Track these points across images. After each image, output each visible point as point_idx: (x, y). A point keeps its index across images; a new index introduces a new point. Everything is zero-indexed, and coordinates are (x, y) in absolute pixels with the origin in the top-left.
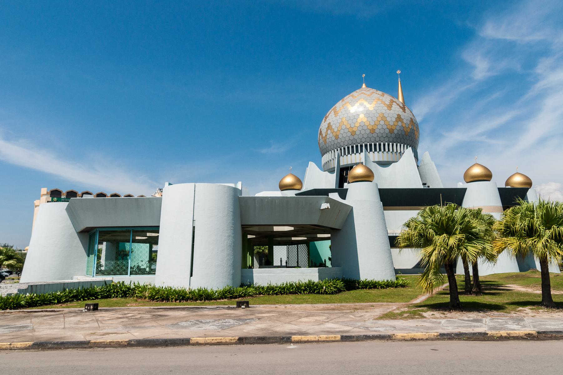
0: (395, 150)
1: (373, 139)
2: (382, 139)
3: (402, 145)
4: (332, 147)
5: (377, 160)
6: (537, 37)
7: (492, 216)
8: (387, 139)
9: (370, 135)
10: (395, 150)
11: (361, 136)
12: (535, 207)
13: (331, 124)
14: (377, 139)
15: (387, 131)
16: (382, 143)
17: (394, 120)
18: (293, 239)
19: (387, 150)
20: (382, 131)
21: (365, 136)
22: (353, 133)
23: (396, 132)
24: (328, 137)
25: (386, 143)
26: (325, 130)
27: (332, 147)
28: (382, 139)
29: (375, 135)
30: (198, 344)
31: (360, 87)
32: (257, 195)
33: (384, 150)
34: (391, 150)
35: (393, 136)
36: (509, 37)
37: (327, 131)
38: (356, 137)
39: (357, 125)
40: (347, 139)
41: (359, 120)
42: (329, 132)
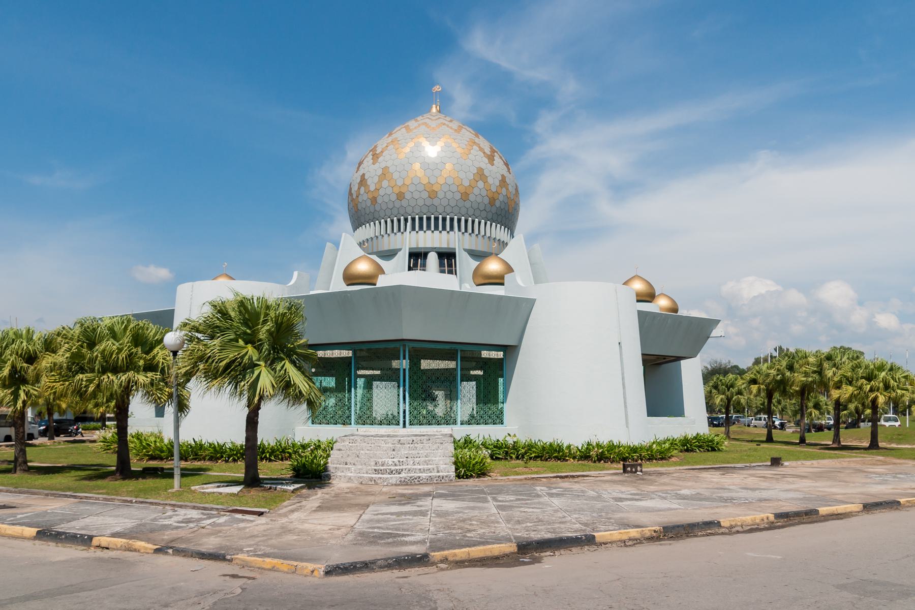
0: (482, 233)
1: (463, 211)
2: (477, 213)
3: (489, 222)
4: (388, 213)
5: (467, 247)
6: (539, 75)
7: (862, 353)
8: (484, 214)
9: (461, 204)
10: (482, 233)
11: (445, 203)
12: (255, 301)
13: (391, 170)
14: (471, 212)
15: (486, 201)
16: (470, 219)
17: (498, 184)
18: (472, 373)
19: (470, 230)
20: (479, 200)
21: (453, 204)
22: (433, 194)
23: (498, 204)
24: (382, 192)
25: (477, 220)
26: (376, 179)
27: (382, 214)
28: (477, 213)
29: (468, 204)
30: (731, 531)
31: (430, 110)
32: (312, 293)
33: (466, 230)
34: (476, 232)
35: (494, 210)
36: (505, 64)
37: (380, 181)
38: (436, 202)
39: (441, 181)
40: (421, 203)
41: (445, 174)
42: (385, 183)
